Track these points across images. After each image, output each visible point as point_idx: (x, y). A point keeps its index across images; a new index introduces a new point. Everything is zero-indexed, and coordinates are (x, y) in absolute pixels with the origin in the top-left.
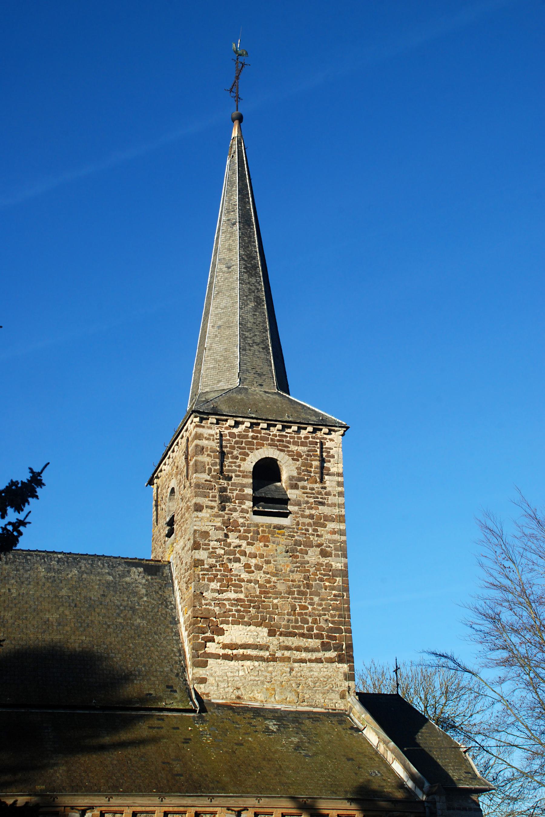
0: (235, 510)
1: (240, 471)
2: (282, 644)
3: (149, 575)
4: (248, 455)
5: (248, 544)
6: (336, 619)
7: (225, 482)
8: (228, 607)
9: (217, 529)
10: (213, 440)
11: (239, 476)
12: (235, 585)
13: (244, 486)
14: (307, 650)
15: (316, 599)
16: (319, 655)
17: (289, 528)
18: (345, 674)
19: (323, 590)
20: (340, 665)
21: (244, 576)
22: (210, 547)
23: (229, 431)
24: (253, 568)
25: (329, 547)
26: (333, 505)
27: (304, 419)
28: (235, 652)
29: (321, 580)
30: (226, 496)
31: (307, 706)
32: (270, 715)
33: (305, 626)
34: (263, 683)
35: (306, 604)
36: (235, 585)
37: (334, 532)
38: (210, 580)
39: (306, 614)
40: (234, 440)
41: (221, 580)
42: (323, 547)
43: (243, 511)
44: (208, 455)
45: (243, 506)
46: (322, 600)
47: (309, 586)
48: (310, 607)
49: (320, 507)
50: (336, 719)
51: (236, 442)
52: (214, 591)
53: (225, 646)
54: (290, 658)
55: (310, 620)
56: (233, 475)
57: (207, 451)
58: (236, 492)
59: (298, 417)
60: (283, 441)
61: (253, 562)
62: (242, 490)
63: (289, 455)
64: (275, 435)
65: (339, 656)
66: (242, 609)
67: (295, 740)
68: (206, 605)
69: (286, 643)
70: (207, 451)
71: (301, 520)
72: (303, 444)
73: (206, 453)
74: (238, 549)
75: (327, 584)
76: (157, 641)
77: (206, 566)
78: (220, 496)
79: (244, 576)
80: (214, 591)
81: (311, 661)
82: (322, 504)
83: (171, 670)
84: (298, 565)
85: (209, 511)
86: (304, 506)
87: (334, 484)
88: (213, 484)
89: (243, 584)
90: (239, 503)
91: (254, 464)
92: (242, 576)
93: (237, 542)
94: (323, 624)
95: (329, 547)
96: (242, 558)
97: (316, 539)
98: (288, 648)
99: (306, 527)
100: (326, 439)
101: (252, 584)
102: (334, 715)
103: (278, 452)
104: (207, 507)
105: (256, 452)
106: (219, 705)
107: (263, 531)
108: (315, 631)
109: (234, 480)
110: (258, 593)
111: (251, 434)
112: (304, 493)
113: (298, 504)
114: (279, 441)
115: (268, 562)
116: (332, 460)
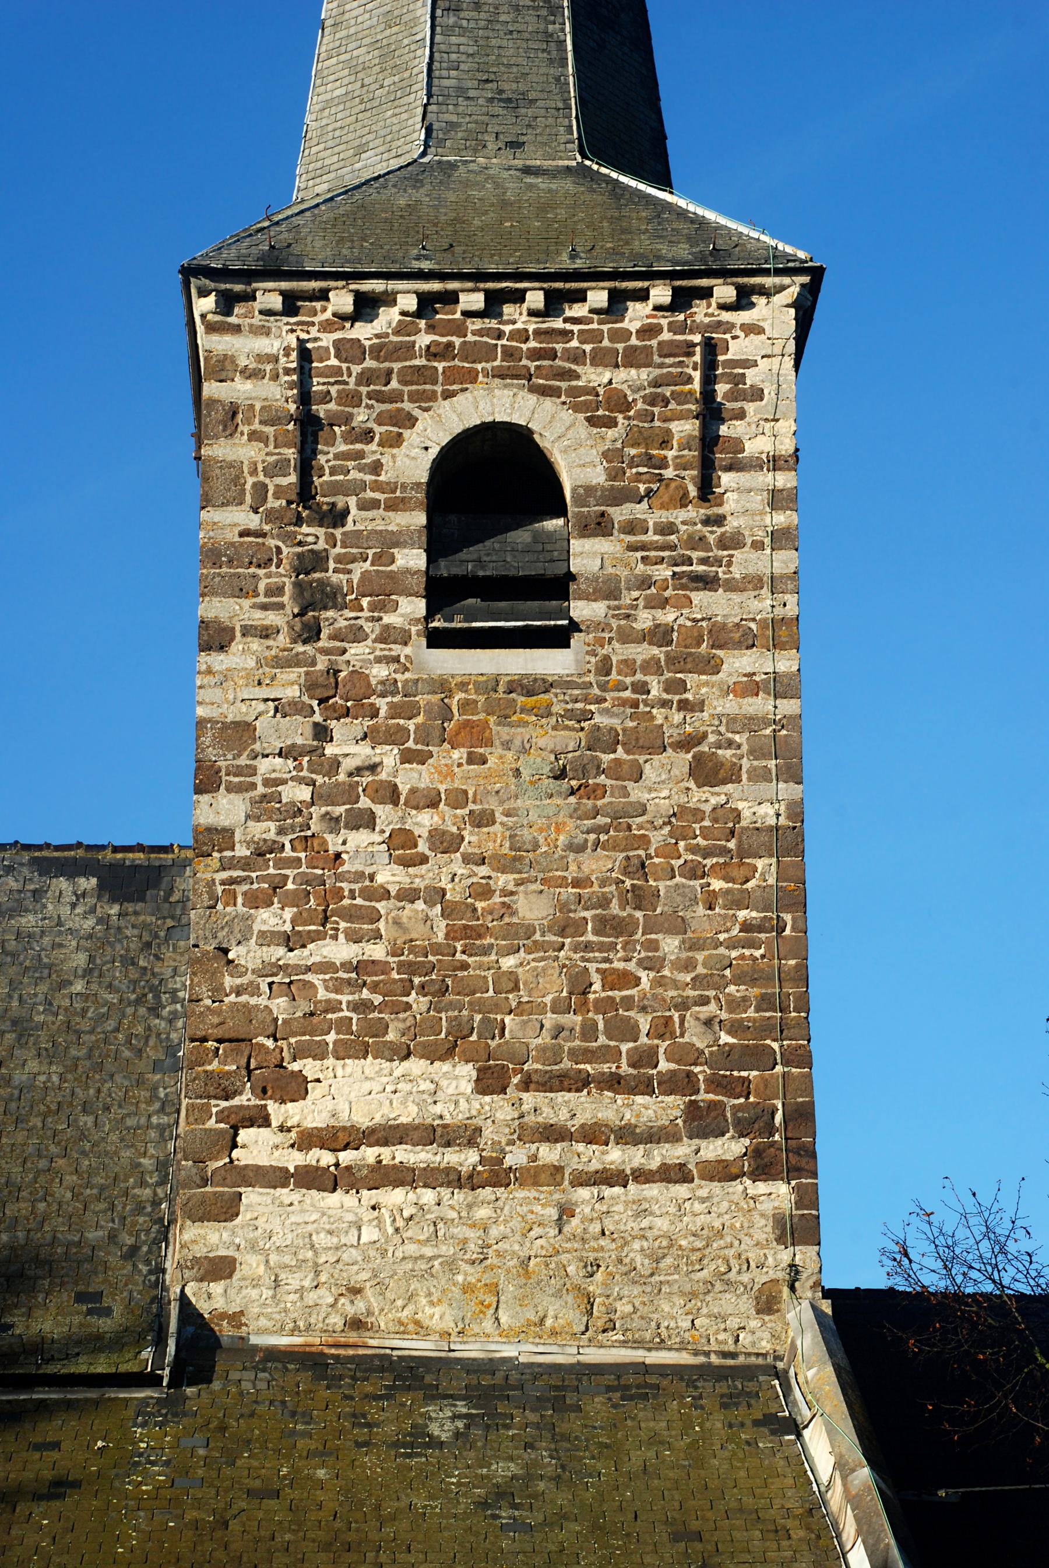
0: (357, 635)
1: (377, 487)
2: (530, 1119)
3: (113, 900)
4: (411, 421)
5: (408, 757)
6: (751, 1013)
7: (321, 531)
8: (322, 994)
9: (281, 708)
10: (275, 377)
11: (374, 504)
12: (350, 915)
13: (392, 541)
14: (627, 1135)
15: (670, 945)
16: (679, 1152)
17: (569, 685)
18: (779, 1221)
19: (701, 910)
20: (762, 1187)
21: (389, 876)
22: (258, 780)
23: (338, 335)
24: (423, 847)
25: (730, 744)
26: (753, 583)
27: (635, 257)
28: (346, 1157)
29: (694, 872)
30: (322, 583)
31: (624, 1344)
32: (459, 1383)
33: (625, 1047)
34: (451, 1266)
35: (631, 966)
36: (350, 915)
37: (750, 687)
38: (256, 901)
39: (628, 1003)
40: (356, 369)
41: (298, 899)
42: (704, 748)
43: (387, 636)
44: (254, 436)
45: (388, 619)
46: (695, 946)
47: (640, 898)
48: (645, 977)
49: (698, 597)
50: (722, 1388)
51: (366, 378)
52: (267, 938)
53: (308, 1140)
54: (558, 1169)
55: (644, 1023)
56: (352, 501)
57: (248, 422)
58: (359, 569)
59: (615, 252)
60: (553, 355)
61: (423, 822)
62: (385, 558)
63: (576, 408)
64: (522, 336)
65: (757, 1153)
66: (378, 999)
67: (503, 1470)
68: (239, 991)
69: (548, 1116)
70: (248, 422)
71: (619, 652)
72: (634, 358)
73: (246, 429)
74: (366, 779)
75: (717, 884)
76: (83, 1136)
77: (242, 851)
78: (297, 585)
79: (389, 876)
80: (267, 938)
81: (642, 1176)
82: (707, 582)
83: (112, 1237)
84: (601, 820)
85: (255, 644)
86: (627, 598)
87: (758, 501)
88: (272, 542)
89: (381, 906)
90: (373, 608)
91: (434, 452)
92: (380, 879)
93: (363, 752)
94: (695, 1037)
95: (730, 744)
96: (383, 812)
97: (677, 717)
98: (552, 1134)
99: (639, 676)
100: (729, 327)
101: (420, 905)
102: (720, 1374)
103: (533, 398)
104: (246, 631)
105: (444, 407)
106: (273, 1354)
107: (466, 706)
108: (664, 1065)
109: (357, 520)
110: (440, 937)
111: (424, 339)
112: (632, 548)
113: (608, 590)
114: (536, 355)
115: (482, 820)
116: (750, 408)
